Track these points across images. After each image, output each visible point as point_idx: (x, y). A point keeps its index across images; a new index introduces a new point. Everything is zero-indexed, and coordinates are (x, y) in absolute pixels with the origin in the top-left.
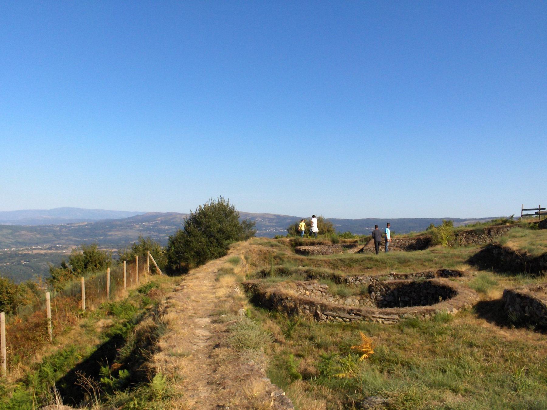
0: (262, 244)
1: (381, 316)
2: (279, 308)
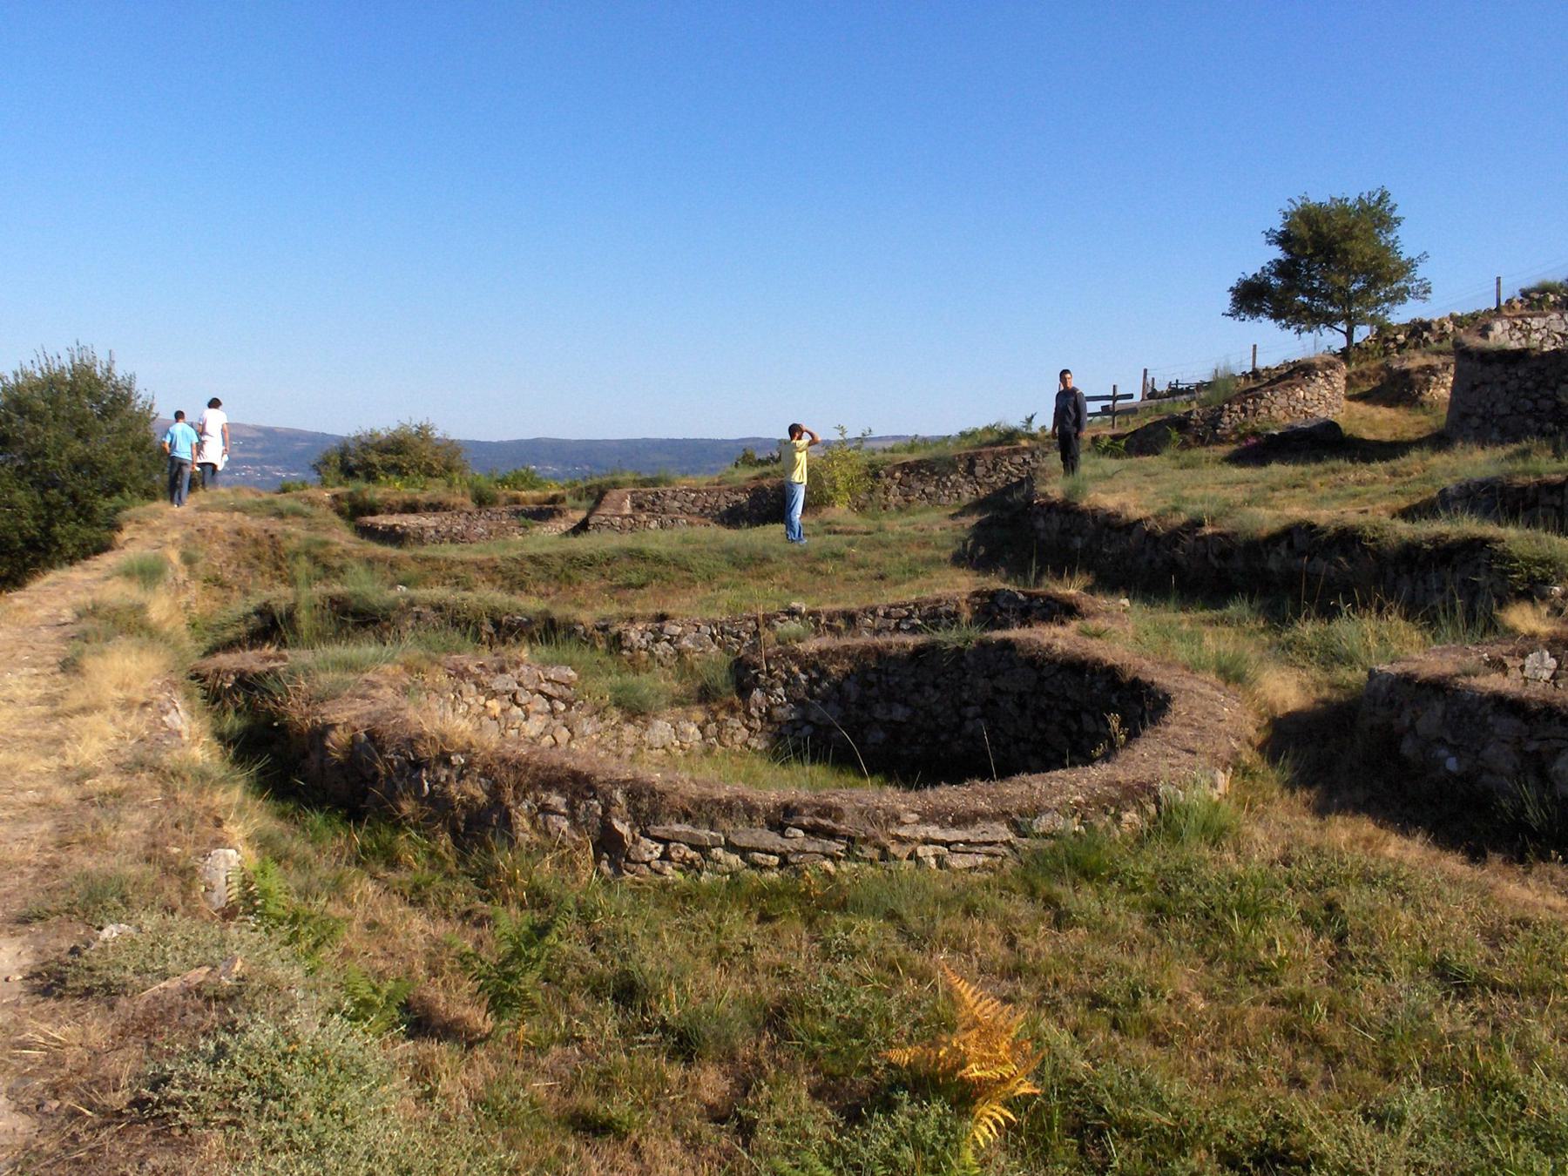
0: (243, 510)
1: (935, 832)
2: (407, 807)
